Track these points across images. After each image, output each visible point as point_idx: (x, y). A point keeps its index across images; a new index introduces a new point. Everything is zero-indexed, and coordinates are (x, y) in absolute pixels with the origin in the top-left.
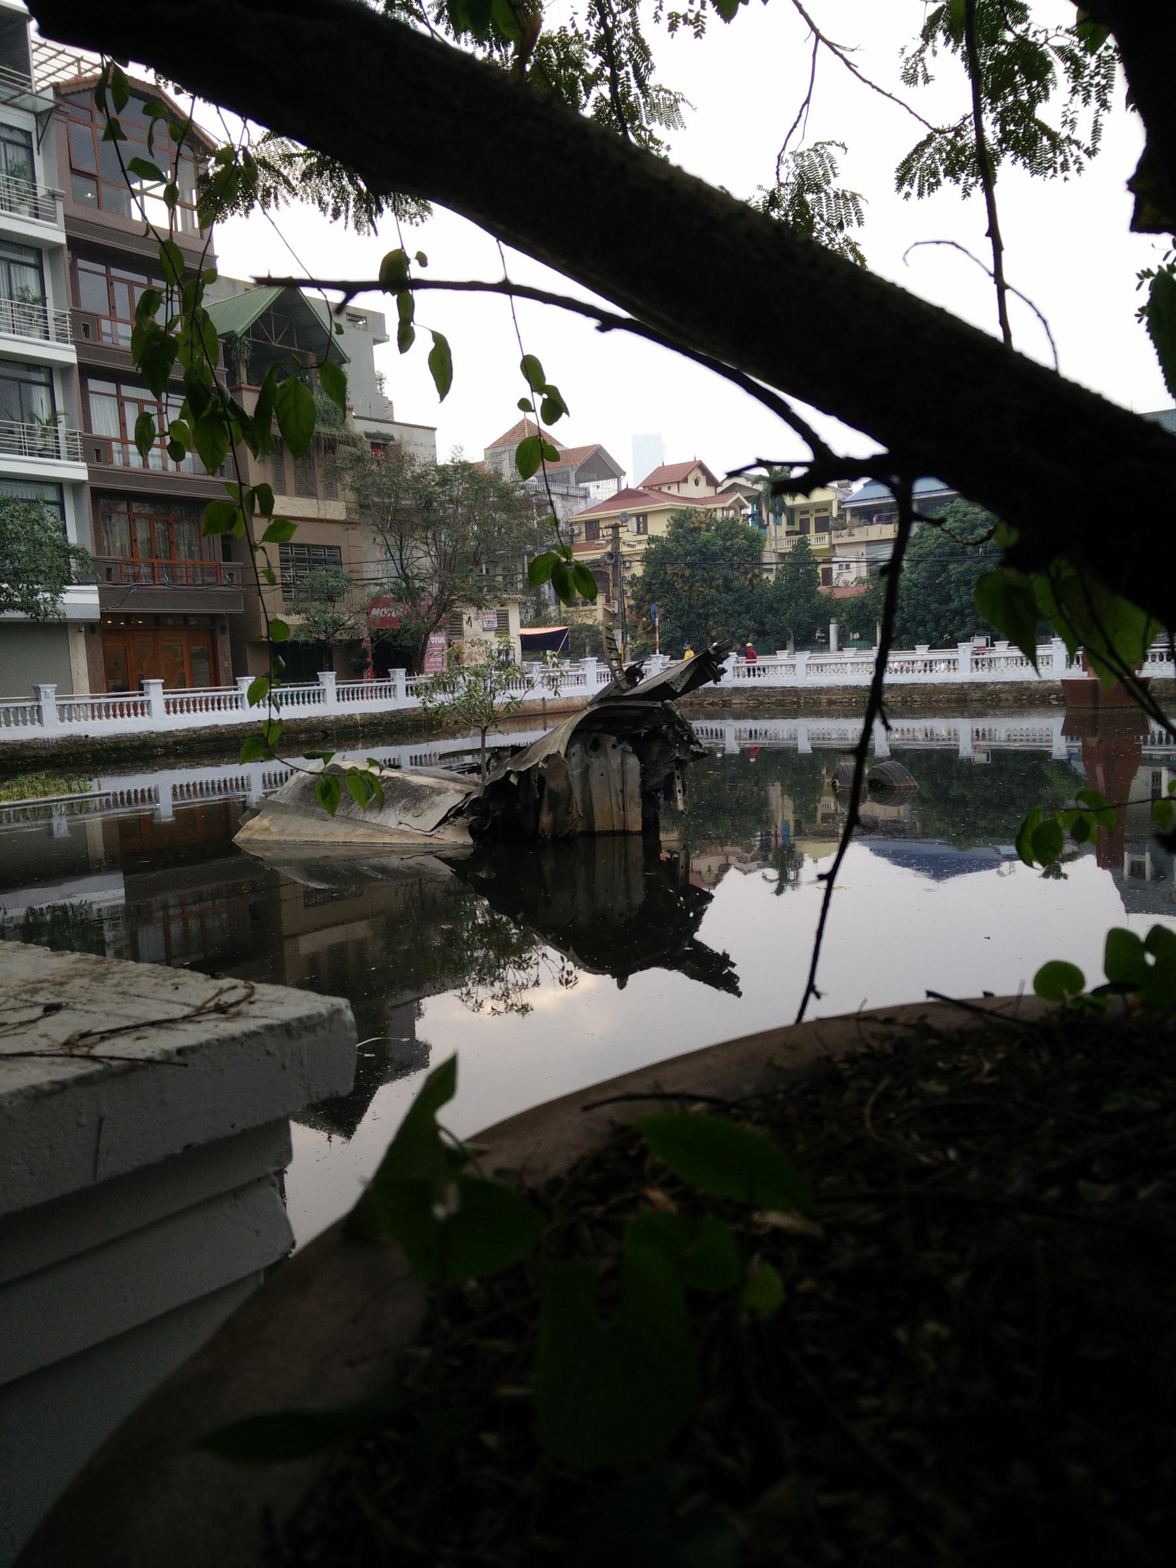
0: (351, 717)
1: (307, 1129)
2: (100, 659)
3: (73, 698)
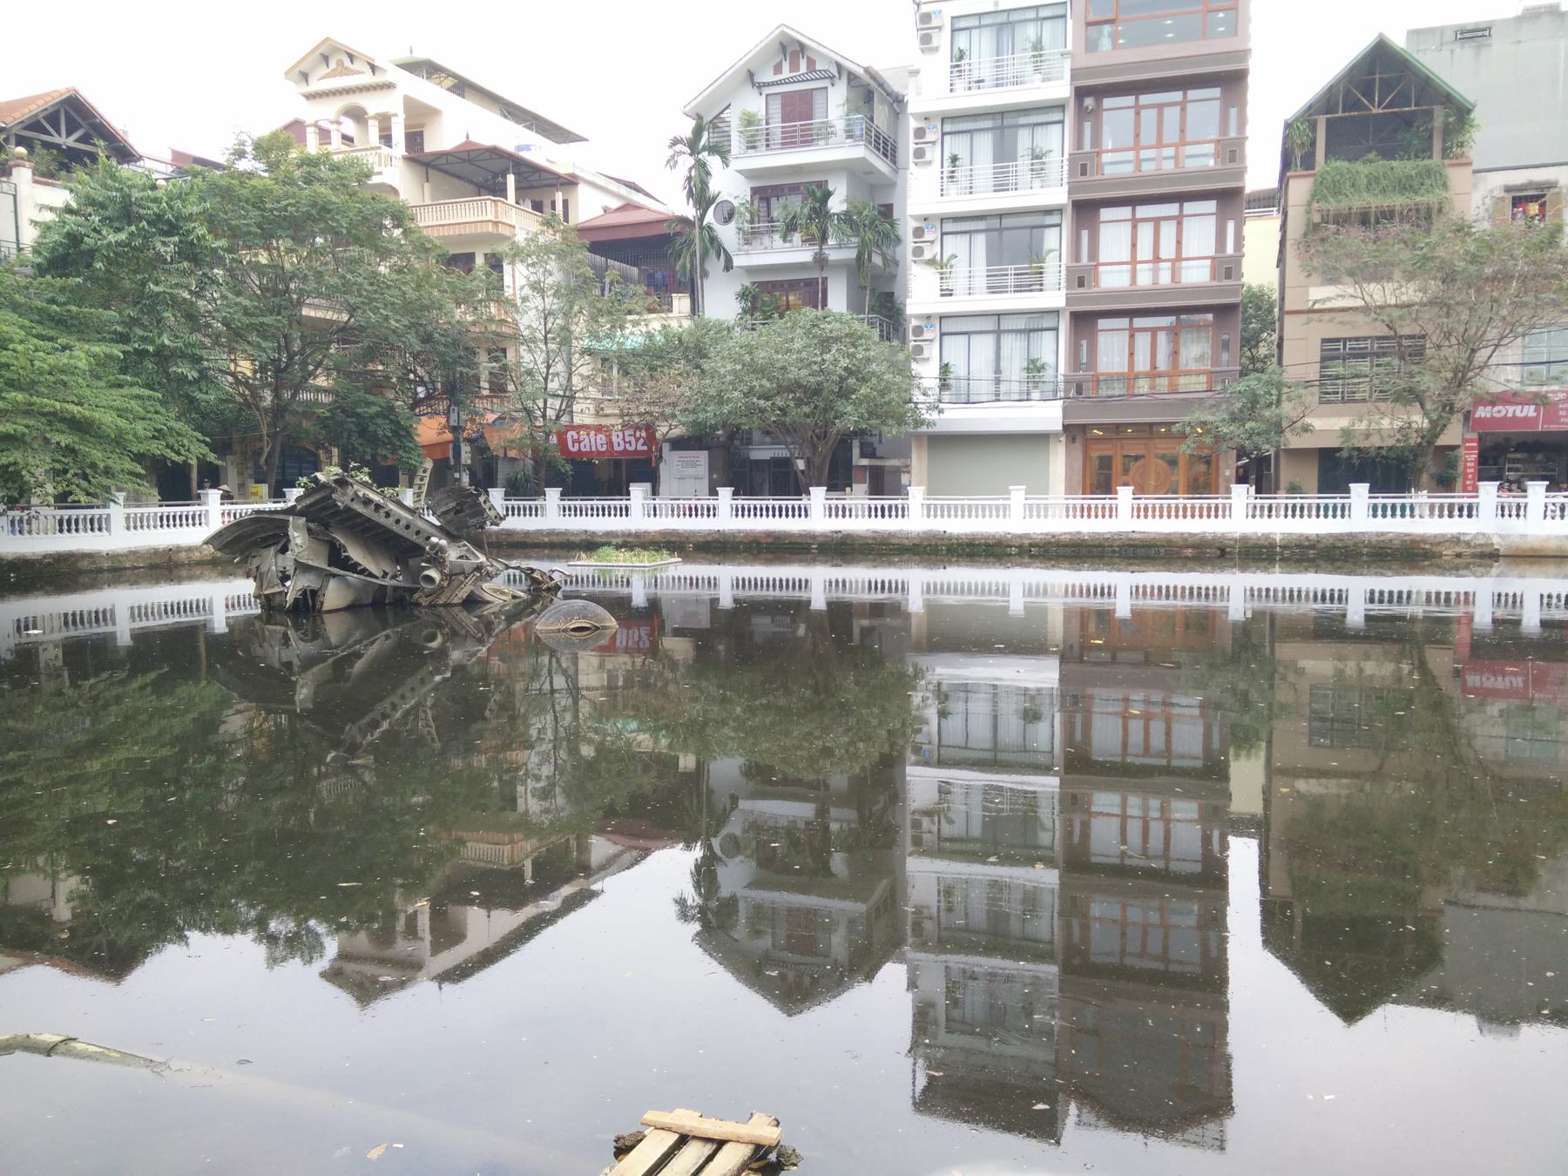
0: (1267, 536)
1: (1230, 872)
2: (1078, 464)
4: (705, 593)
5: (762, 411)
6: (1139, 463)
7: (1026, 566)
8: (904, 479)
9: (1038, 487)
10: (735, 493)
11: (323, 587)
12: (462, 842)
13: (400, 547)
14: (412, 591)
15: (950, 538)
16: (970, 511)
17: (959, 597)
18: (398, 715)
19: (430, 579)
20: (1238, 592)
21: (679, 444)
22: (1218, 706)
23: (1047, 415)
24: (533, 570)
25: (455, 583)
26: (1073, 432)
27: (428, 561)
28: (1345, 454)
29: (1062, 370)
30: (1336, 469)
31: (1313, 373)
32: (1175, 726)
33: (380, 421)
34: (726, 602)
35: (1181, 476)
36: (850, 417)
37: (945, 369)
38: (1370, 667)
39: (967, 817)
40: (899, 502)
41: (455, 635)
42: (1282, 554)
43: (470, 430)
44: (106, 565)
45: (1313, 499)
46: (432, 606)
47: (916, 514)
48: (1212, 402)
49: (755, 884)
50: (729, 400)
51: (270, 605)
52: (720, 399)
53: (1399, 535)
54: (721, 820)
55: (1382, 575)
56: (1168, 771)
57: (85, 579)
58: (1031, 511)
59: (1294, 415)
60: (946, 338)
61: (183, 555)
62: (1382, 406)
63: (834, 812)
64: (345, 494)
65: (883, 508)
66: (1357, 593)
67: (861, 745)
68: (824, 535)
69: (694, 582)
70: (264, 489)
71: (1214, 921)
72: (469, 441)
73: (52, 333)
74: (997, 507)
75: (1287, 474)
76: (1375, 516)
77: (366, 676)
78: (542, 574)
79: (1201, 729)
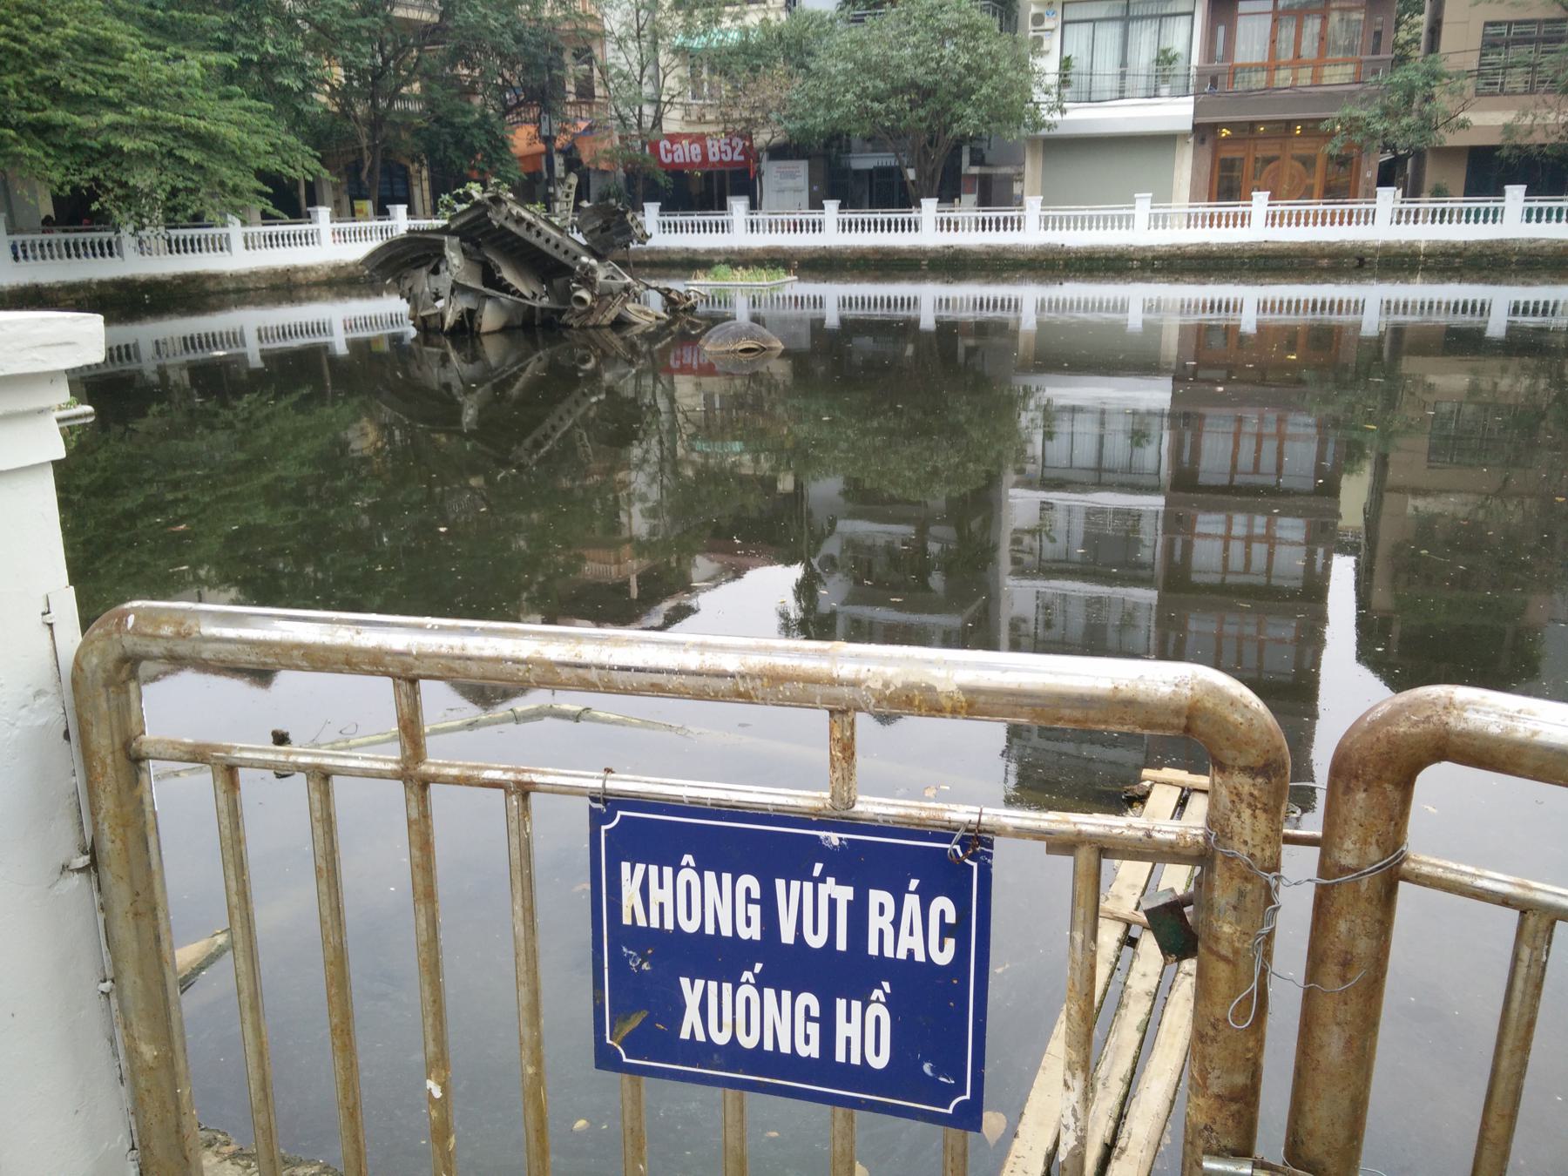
0: (1411, 244)
2: (1206, 169)
4: (809, 312)
5: (875, 115)
6: (1272, 166)
7: (1148, 280)
8: (1017, 189)
9: (1163, 195)
10: (841, 207)
11: (481, 307)
12: (581, 559)
13: (547, 267)
14: (560, 313)
15: (1068, 251)
16: (1091, 223)
18: (558, 435)
19: (581, 301)
20: (1372, 304)
21: (778, 152)
22: (1336, 423)
23: (1176, 112)
24: (670, 291)
25: (604, 303)
26: (1202, 131)
27: (578, 282)
28: (1505, 153)
29: (1195, 61)
30: (1487, 171)
31: (1473, 62)
32: (1287, 446)
33: (475, 131)
34: (832, 319)
35: (1317, 182)
36: (970, 119)
37: (1066, 63)
38: (1505, 384)
39: (1069, 539)
40: (1015, 214)
41: (605, 358)
42: (1425, 262)
43: (561, 141)
44: (231, 286)
45: (1457, 203)
46: (583, 328)
47: (1033, 228)
48: (1363, 95)
49: (852, 600)
50: (840, 104)
51: (428, 328)
52: (830, 104)
53: (1552, 241)
54: (819, 540)
55: (1529, 284)
56: (1275, 492)
57: (213, 301)
58: (1156, 221)
59: (1450, 108)
60: (1068, 27)
61: (300, 275)
62: (1550, 98)
63: (934, 530)
64: (498, 212)
66: (1499, 304)
67: (971, 466)
68: (935, 250)
69: (798, 301)
70: (368, 206)
71: (1312, 637)
72: (560, 151)
73: (159, 42)
74: (1120, 217)
75: (1431, 176)
76: (1528, 221)
77: (524, 401)
78: (679, 294)
79: (1314, 447)
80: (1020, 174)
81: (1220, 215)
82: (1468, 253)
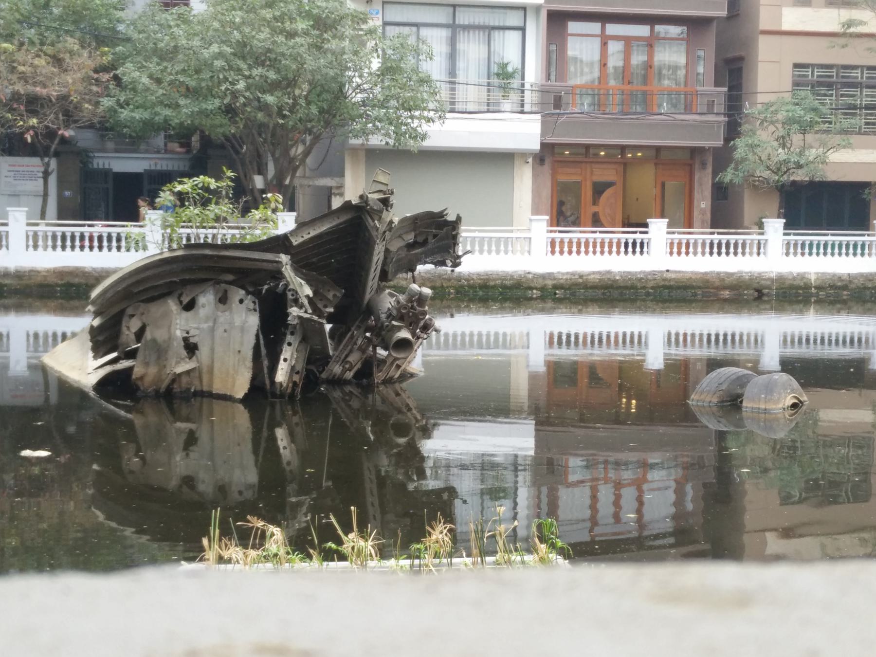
0: (802, 276)
3: (512, 231)
10: (787, 226)
17: (476, 351)
23: (524, 132)
26: (547, 154)
42: (817, 295)
65: (728, 245)
80: (341, 186)
81: (562, 242)
82: (853, 286)
